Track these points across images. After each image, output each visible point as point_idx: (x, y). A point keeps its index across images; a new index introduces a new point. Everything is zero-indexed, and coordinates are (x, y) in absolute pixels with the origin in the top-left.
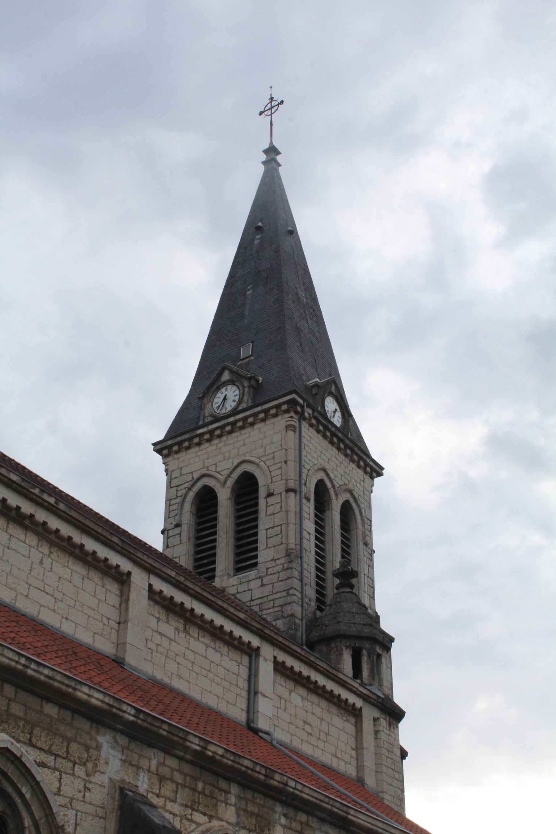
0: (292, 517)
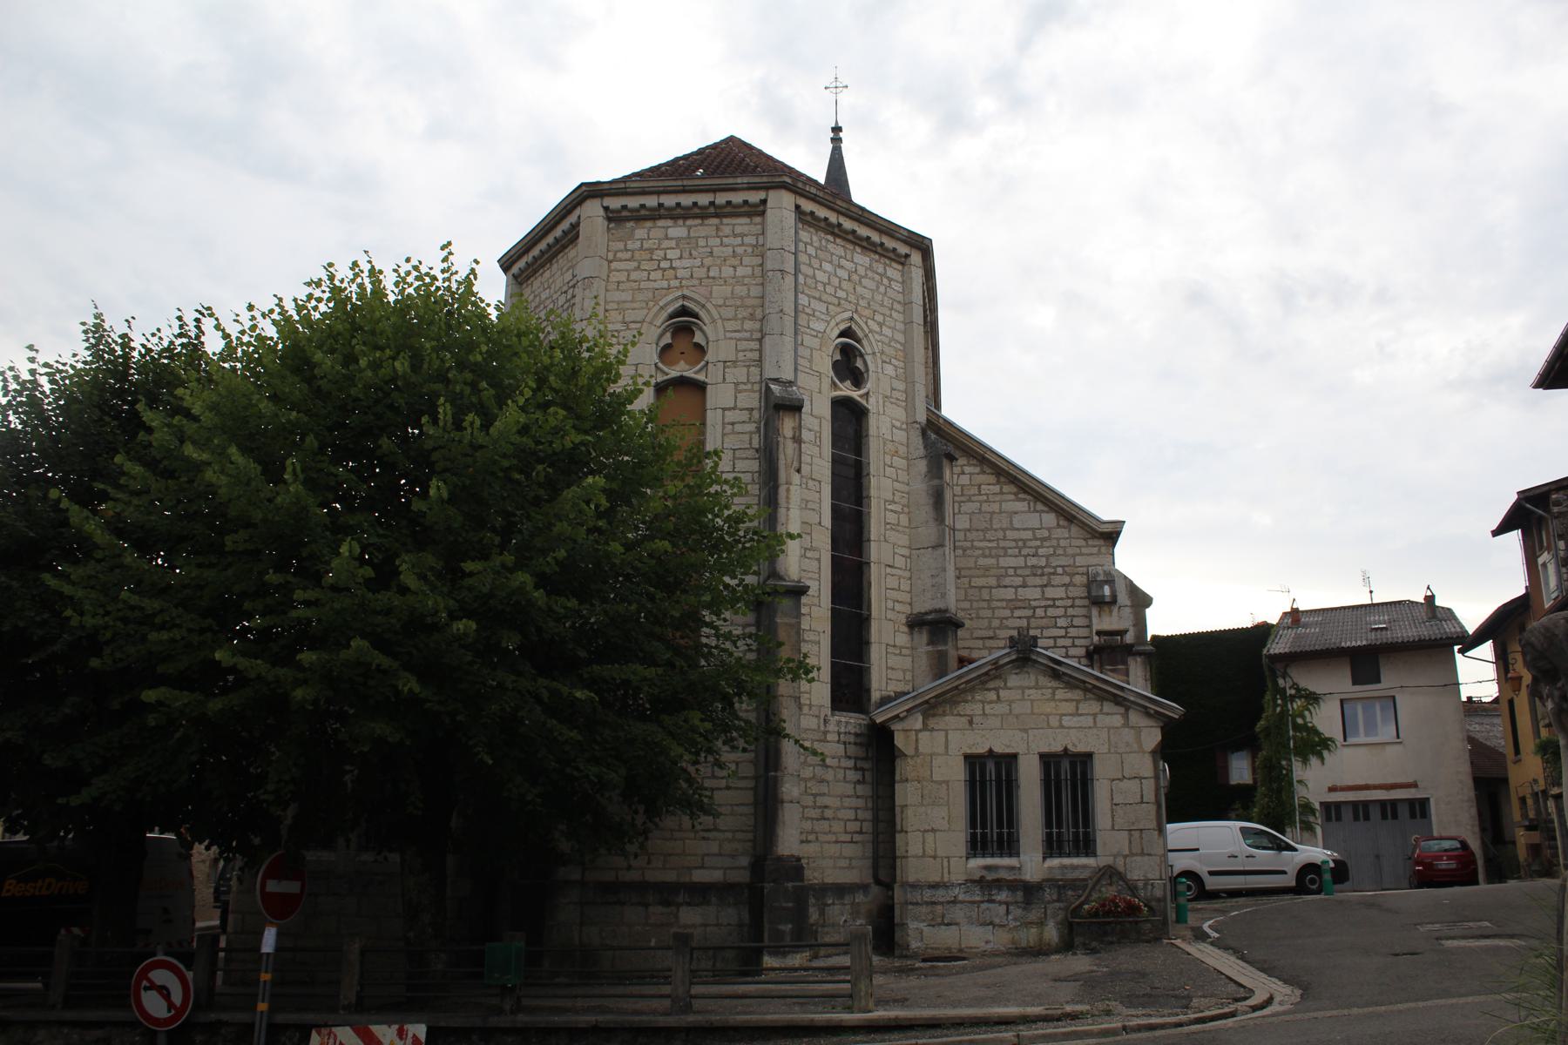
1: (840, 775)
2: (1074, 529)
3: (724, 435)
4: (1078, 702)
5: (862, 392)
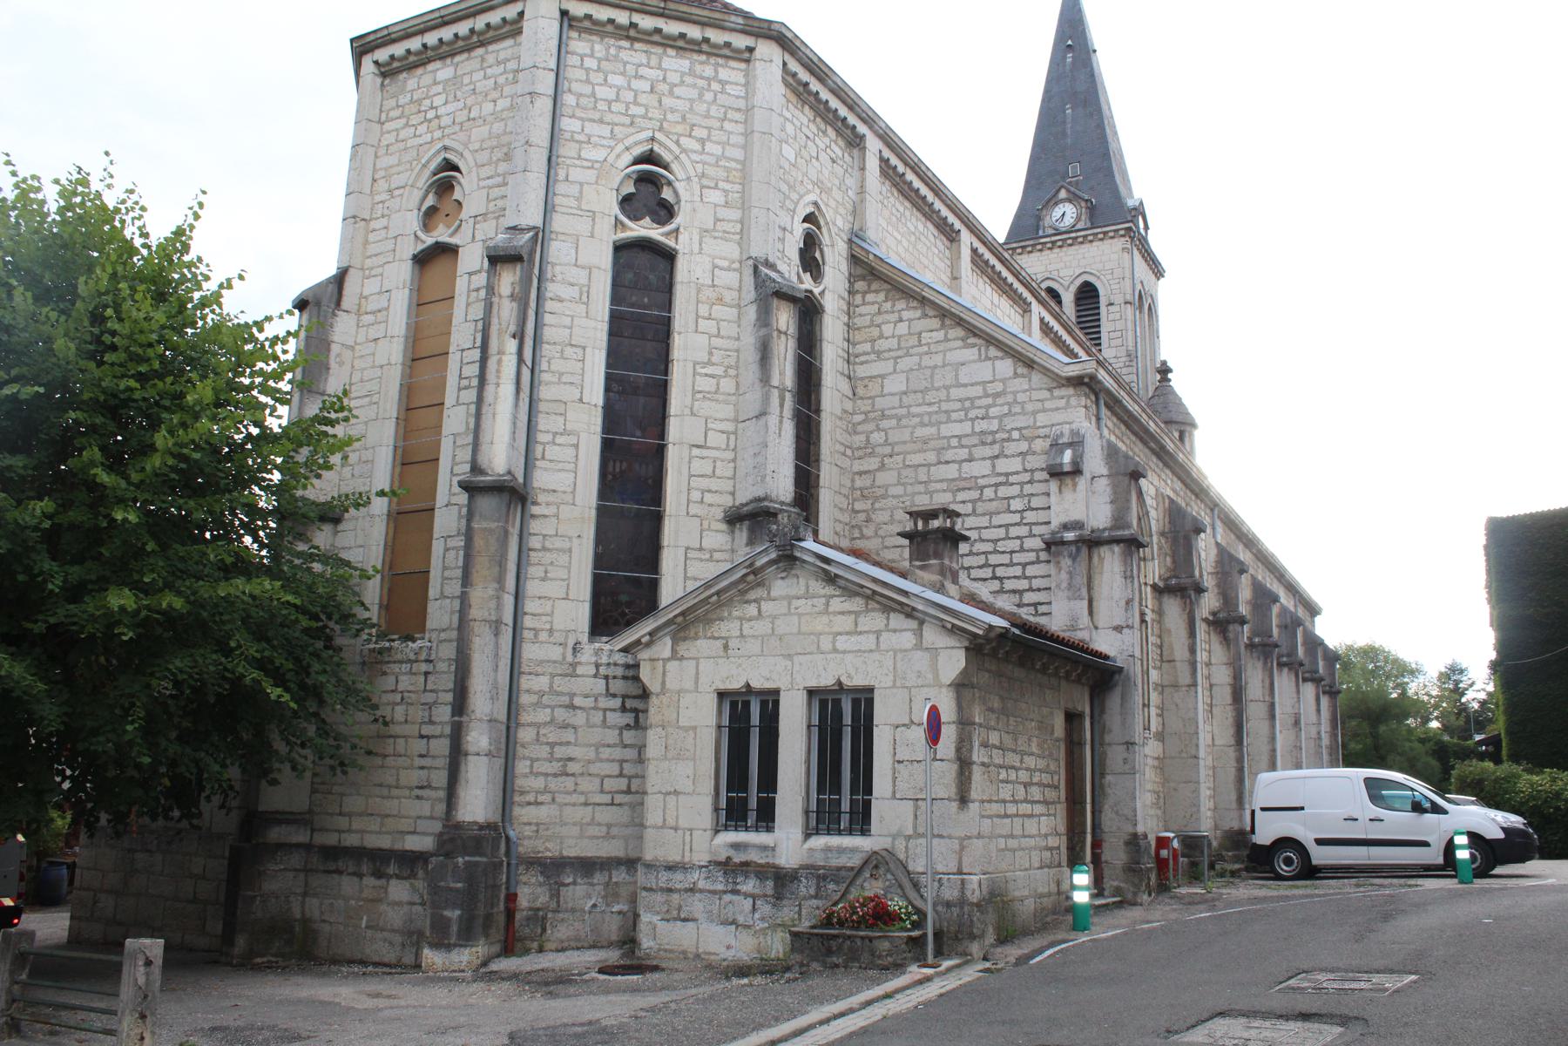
0: (1130, 325)
2: (1036, 377)
3: (468, 305)
4: (857, 614)
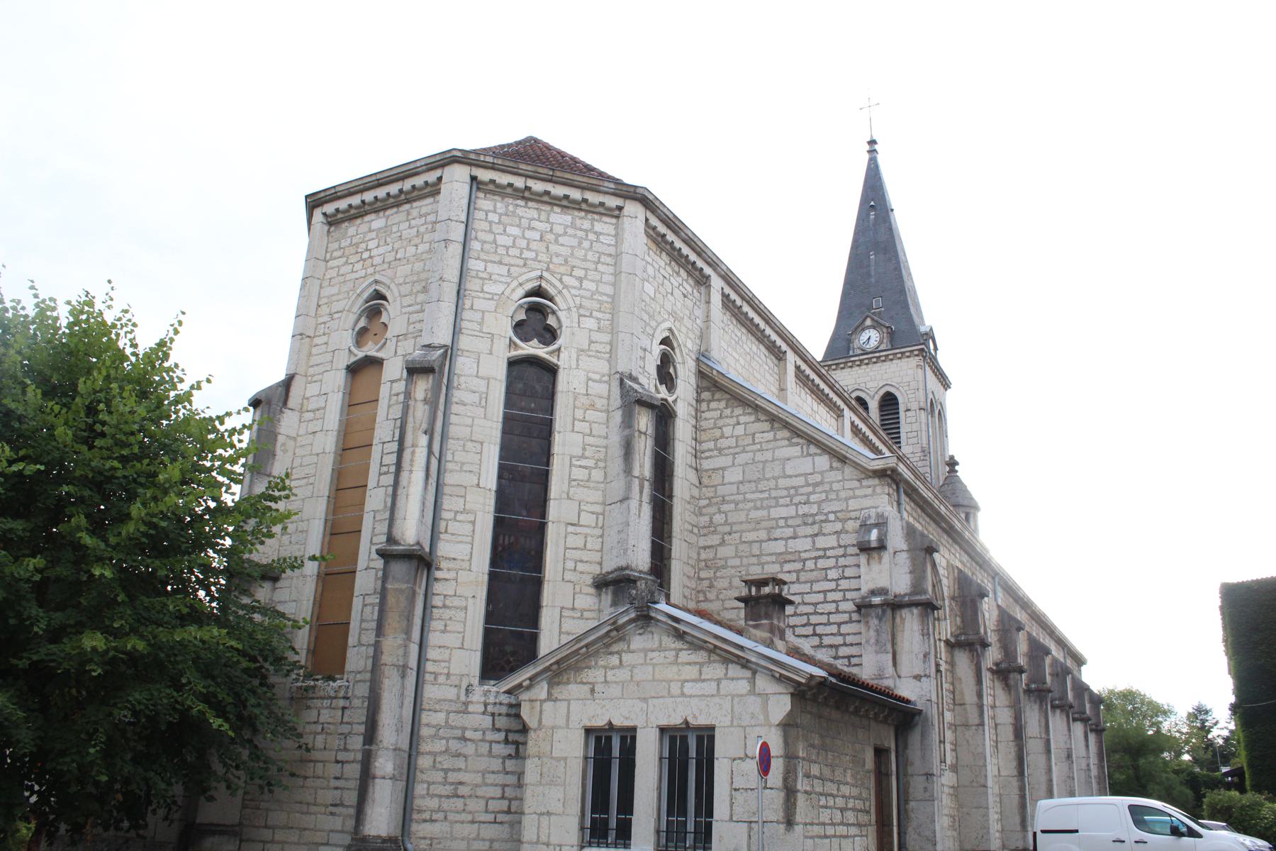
0: (924, 426)
1: (484, 748)
2: (848, 470)
5: (551, 348)
